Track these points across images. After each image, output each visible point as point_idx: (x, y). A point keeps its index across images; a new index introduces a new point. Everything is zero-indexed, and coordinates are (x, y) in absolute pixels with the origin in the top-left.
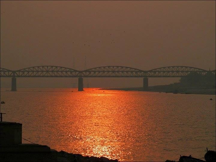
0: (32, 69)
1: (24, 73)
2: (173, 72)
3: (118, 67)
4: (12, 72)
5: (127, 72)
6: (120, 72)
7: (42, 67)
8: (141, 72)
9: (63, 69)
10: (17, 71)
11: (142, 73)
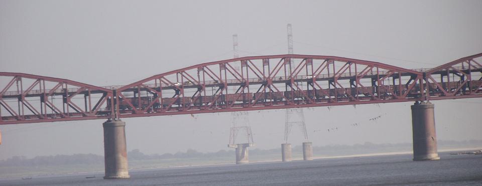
4: (101, 95)
9: (27, 83)
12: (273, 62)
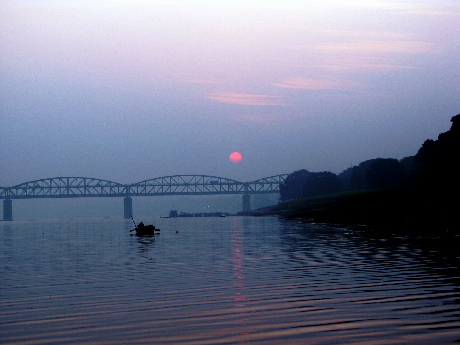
1: (263, 186)
6: (192, 185)
7: (58, 180)
12: (71, 180)
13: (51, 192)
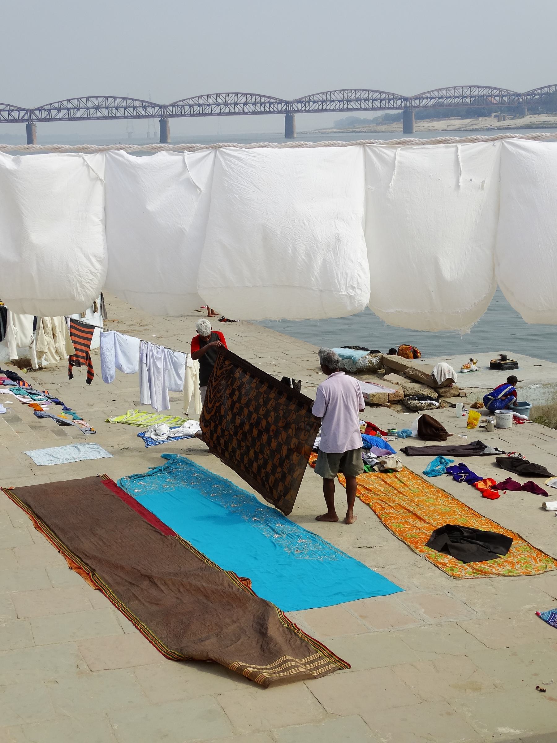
0: (66, 103)
2: (218, 105)
3: (106, 98)
4: (25, 112)
5: (125, 108)
8: (153, 107)
10: (36, 109)
11: (157, 108)
13: (170, 110)
